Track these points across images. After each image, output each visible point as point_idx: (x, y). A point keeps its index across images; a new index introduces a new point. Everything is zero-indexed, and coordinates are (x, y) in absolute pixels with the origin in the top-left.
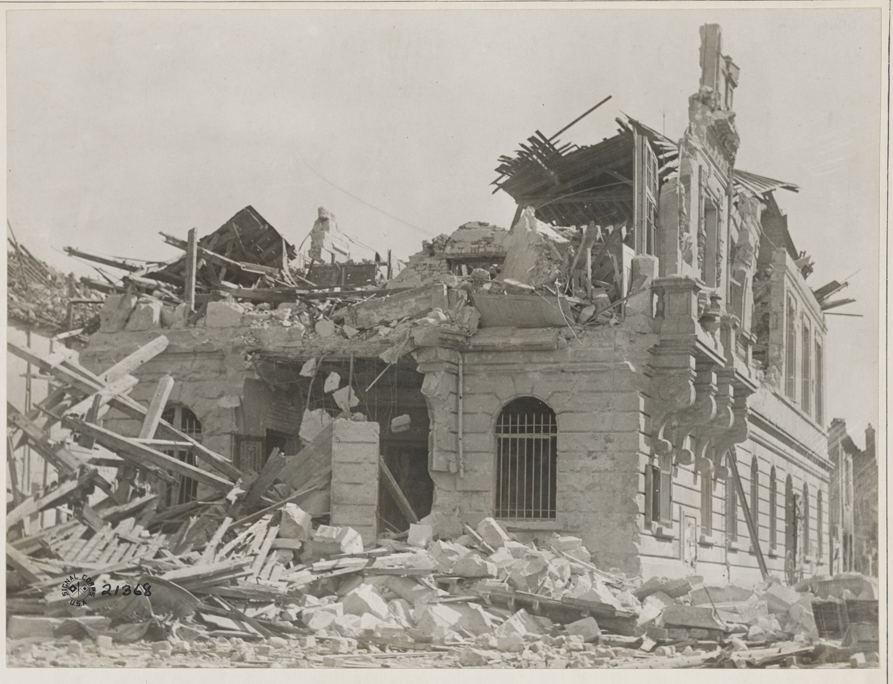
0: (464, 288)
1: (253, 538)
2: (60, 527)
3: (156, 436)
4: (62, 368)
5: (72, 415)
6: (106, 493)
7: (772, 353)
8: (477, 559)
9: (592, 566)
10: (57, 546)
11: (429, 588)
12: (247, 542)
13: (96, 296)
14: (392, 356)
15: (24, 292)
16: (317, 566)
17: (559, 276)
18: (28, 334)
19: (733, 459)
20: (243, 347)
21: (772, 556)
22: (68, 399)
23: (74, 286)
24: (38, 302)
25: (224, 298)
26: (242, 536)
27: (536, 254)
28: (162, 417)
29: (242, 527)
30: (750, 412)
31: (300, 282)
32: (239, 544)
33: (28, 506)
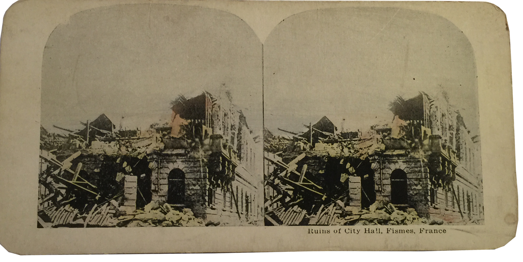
0: (381, 138)
1: (329, 210)
2: (278, 208)
3: (77, 181)
4: (51, 160)
5: (53, 174)
6: (62, 197)
7: (242, 156)
8: (388, 215)
9: (194, 217)
10: (277, 214)
11: (150, 224)
12: (328, 212)
13: (61, 139)
14: (141, 157)
15: (267, 141)
16: (346, 218)
17: (185, 134)
18: (268, 153)
19: (452, 186)
20: (101, 154)
21: (242, 214)
22: (279, 171)
23: (55, 136)
24: (45, 141)
25: (96, 140)
26: (99, 210)
27: (399, 128)
28: (79, 175)
29: (100, 207)
30: (456, 172)
31: (116, 135)
32: (99, 212)
33: (269, 202)
